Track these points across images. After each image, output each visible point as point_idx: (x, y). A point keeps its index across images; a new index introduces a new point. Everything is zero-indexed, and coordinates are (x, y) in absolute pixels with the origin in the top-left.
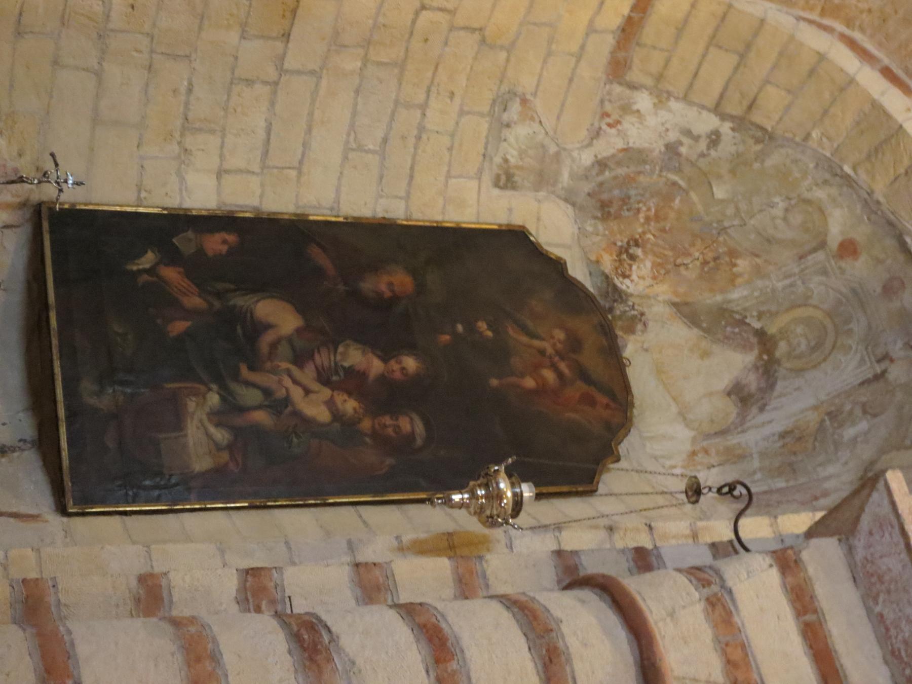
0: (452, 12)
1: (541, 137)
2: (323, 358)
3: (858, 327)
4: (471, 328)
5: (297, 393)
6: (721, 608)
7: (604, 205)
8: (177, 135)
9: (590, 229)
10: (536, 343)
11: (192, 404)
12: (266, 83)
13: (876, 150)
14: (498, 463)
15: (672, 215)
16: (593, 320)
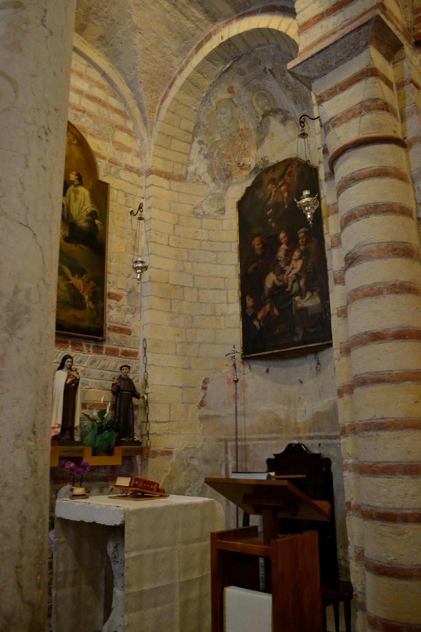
0: (169, 235)
1: (207, 201)
2: (282, 264)
3: (256, 82)
4: (270, 217)
5: (294, 272)
6: (335, 122)
7: (227, 177)
8: (217, 318)
9: (236, 180)
10: (273, 194)
11: (299, 305)
12: (198, 292)
14: (296, 204)
15: (228, 153)
16: (265, 175)
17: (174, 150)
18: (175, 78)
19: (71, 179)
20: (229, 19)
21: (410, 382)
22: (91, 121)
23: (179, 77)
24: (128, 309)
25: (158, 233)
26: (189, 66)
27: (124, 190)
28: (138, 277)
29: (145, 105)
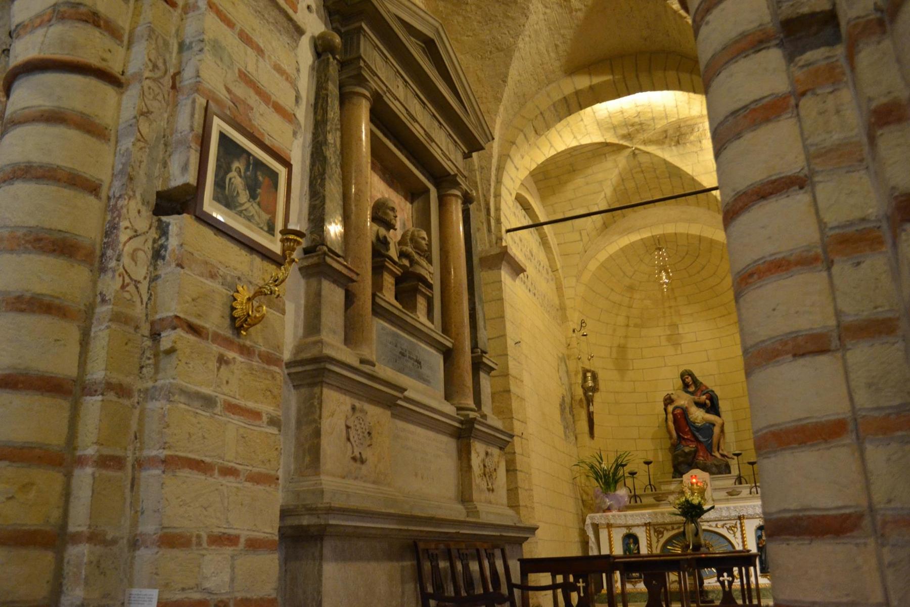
21: (7, 463)
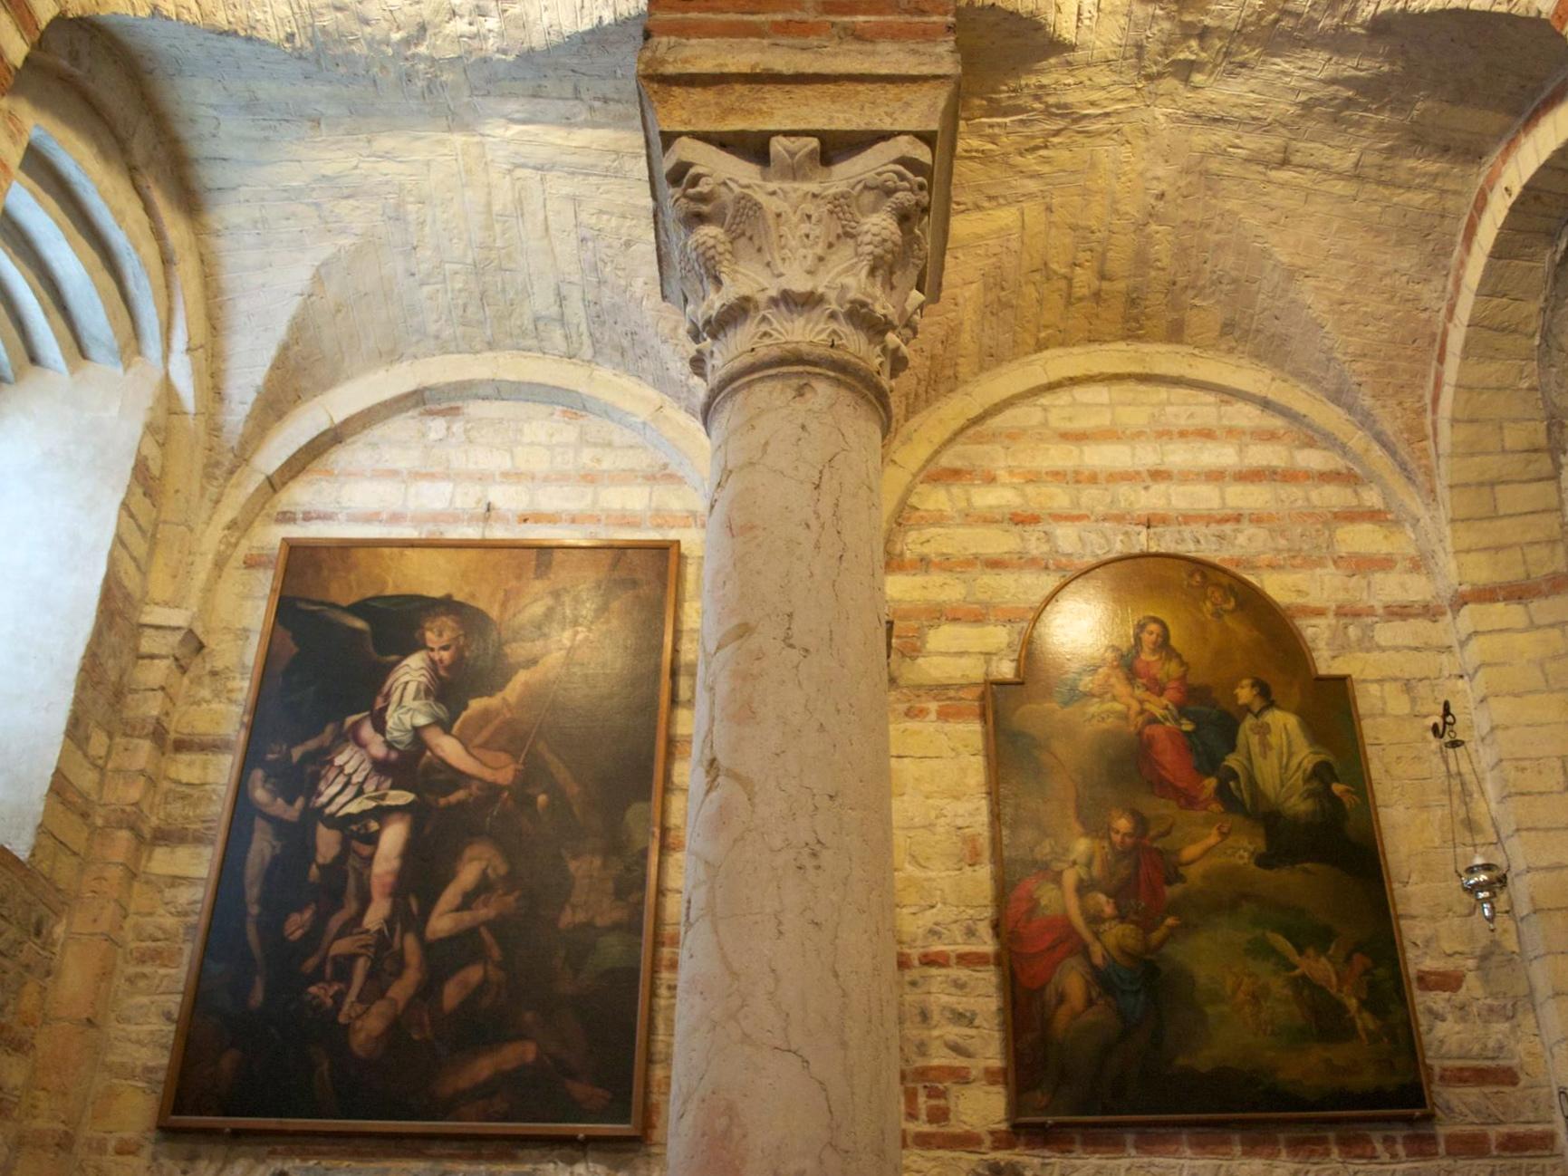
13: (1503, 330)
17: (1511, 516)
18: (1445, 334)
19: (1241, 702)
20: (1509, 136)
22: (1261, 534)
23: (1450, 326)
24: (1491, 1009)
25: (1526, 764)
26: (1464, 289)
27: (1399, 674)
28: (1487, 913)
29: (1390, 432)
